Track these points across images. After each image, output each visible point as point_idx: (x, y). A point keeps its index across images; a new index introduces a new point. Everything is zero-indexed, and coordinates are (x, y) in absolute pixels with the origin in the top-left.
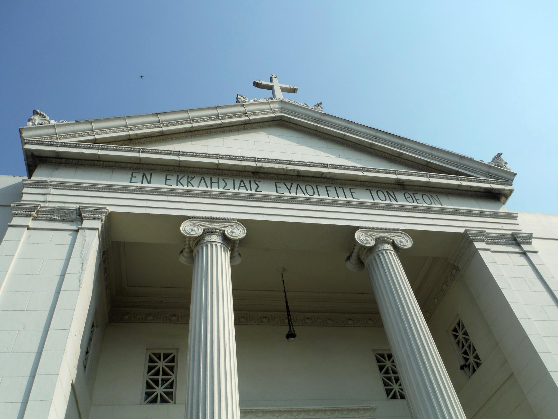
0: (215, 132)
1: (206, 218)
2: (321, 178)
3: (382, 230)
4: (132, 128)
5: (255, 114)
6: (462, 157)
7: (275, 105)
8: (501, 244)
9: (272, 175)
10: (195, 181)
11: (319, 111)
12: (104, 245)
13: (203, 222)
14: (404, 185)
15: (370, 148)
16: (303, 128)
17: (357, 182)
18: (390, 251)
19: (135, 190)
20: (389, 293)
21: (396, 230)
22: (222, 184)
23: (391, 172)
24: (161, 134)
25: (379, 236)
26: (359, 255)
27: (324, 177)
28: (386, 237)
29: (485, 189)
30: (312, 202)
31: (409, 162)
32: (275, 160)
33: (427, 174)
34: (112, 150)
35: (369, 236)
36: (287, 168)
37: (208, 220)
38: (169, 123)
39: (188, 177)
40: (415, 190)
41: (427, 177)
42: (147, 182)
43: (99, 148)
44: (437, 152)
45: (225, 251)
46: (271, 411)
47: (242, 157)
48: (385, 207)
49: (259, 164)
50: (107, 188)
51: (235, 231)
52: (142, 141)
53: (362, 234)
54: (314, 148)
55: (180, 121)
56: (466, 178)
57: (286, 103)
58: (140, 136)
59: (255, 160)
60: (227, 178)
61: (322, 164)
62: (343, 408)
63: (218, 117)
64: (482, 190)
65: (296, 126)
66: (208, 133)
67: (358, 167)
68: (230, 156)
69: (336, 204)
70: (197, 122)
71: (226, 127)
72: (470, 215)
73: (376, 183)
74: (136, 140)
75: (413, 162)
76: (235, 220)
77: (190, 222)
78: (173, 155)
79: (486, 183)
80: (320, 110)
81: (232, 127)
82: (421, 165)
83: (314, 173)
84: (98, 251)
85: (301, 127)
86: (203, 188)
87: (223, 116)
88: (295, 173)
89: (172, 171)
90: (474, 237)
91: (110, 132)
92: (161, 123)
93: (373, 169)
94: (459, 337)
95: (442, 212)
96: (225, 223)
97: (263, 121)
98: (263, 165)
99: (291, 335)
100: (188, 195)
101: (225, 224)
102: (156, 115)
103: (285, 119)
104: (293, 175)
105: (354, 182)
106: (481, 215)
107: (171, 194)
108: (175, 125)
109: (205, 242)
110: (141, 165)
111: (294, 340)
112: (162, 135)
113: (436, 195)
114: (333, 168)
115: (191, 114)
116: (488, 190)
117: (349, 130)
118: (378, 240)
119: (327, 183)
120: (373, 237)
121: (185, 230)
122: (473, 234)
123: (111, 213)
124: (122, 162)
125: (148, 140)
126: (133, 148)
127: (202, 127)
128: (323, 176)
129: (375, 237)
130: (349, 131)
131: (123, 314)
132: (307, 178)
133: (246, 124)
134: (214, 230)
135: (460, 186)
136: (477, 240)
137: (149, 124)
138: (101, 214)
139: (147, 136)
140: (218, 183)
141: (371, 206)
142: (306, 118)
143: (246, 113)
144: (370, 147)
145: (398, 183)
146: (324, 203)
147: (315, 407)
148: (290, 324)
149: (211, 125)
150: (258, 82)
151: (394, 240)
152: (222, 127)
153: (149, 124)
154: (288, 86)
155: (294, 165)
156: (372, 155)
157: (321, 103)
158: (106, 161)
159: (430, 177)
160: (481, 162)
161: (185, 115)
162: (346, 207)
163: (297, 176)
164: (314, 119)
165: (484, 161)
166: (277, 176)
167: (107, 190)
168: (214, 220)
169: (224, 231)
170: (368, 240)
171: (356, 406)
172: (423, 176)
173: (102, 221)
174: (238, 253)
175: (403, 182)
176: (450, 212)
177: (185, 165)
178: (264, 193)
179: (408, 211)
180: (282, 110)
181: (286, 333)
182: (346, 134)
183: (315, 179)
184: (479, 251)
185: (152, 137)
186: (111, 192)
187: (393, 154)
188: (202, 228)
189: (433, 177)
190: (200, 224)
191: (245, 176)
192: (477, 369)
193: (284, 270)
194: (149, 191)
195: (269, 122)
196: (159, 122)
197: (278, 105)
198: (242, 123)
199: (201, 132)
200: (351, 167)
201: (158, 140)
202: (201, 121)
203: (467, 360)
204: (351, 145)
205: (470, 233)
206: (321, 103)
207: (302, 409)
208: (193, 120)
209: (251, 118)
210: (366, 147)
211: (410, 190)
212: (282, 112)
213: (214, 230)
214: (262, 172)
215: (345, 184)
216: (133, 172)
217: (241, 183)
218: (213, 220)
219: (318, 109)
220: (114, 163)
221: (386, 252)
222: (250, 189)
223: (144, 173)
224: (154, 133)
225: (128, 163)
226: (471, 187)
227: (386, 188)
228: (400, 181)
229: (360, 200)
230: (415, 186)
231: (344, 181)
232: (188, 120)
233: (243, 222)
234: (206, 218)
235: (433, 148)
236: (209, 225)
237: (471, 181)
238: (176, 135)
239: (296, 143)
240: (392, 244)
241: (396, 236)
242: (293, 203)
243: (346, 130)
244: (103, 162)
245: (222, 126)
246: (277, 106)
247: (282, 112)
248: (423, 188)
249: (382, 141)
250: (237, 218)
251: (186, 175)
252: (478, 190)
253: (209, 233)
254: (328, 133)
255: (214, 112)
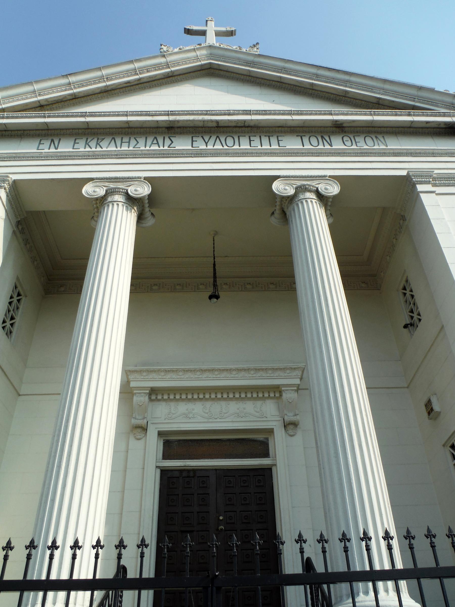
0: (134, 90)
1: (110, 178)
2: (245, 127)
3: (306, 177)
4: (41, 93)
5: (178, 64)
6: (420, 88)
7: (201, 51)
8: (452, 186)
9: (188, 129)
10: (104, 143)
11: (254, 53)
12: (16, 214)
13: (107, 183)
14: (343, 127)
15: (311, 89)
16: (235, 75)
17: (286, 129)
18: (312, 200)
19: (39, 156)
20: (301, 243)
21: (322, 177)
22: (133, 142)
23: (326, 113)
24: (74, 97)
25: (299, 184)
26: (283, 208)
27: (247, 125)
28: (307, 185)
29: (445, 123)
30: (229, 154)
31: (357, 101)
32: (191, 111)
33: (371, 111)
34: (18, 118)
35: (289, 185)
36: (203, 119)
37: (113, 180)
38: (80, 84)
39: (98, 139)
40: (357, 132)
41: (371, 115)
42: (54, 148)
43: (4, 117)
44: (390, 85)
45: (127, 210)
46: (192, 371)
47: (154, 111)
48: (314, 152)
49: (172, 118)
50: (12, 157)
51: (138, 189)
52: (54, 106)
53: (281, 183)
54: (245, 96)
55: (93, 81)
56: (421, 112)
57: (215, 47)
58: (51, 101)
59: (169, 114)
60: (139, 136)
61: (244, 111)
62: (268, 367)
63: (135, 72)
64: (442, 126)
65: (227, 73)
66: (126, 91)
67: (287, 111)
68: (140, 112)
69: (257, 153)
70: (112, 79)
71: (146, 82)
72: (420, 155)
73: (308, 127)
74: (48, 106)
75: (362, 100)
76: (140, 178)
77: (93, 184)
78: (80, 117)
79: (447, 117)
80: (254, 52)
81: (153, 82)
82: (371, 103)
83: (235, 122)
84: (5, 219)
85: (232, 74)
86: (112, 148)
87: (142, 70)
88: (215, 125)
89: (81, 134)
90: (417, 178)
91: (18, 100)
92: (72, 85)
93: (305, 111)
94: (407, 294)
95: (385, 153)
96: (130, 182)
97: (190, 71)
98: (176, 118)
99: (214, 296)
100: (94, 156)
101: (130, 183)
102: (66, 76)
103: (215, 67)
104: (212, 126)
105: (283, 129)
106: (433, 154)
107: (77, 158)
108: (87, 86)
109: (107, 203)
110: (49, 131)
111: (217, 302)
112: (75, 98)
113: (382, 135)
114: (256, 114)
115: (105, 72)
116: (449, 125)
117: (286, 71)
118: (299, 188)
119: (251, 132)
120: (293, 185)
121: (87, 192)
122: (416, 176)
123: (15, 181)
124: (30, 130)
125: (60, 105)
126: (39, 114)
127: (119, 85)
128: (246, 124)
129: (296, 186)
130: (286, 72)
131: (59, 286)
132: (228, 128)
133: (169, 77)
134: (117, 190)
135: (412, 122)
136: (421, 183)
137: (59, 88)
138: (4, 182)
139: (60, 101)
140: (129, 142)
141: (298, 153)
142: (237, 62)
143: (168, 65)
144: (312, 88)
145: (336, 126)
146: (243, 153)
147: (237, 366)
148: (215, 285)
149: (128, 82)
150: (189, 28)
151: (318, 187)
152: (141, 84)
153: (59, 88)
154: (223, 29)
155: (212, 115)
156: (313, 97)
157: (257, 44)
158: (14, 131)
159: (375, 115)
160: (445, 92)
161: (98, 74)
162: (268, 156)
163: (216, 127)
164: (247, 63)
165: (449, 90)
166: (194, 129)
167: (12, 159)
168: (118, 180)
169: (127, 190)
170: (287, 190)
171: (281, 365)
172: (365, 115)
173: (5, 189)
174: (151, 213)
175: (342, 124)
176: (394, 153)
177: (94, 127)
178: (177, 148)
179: (342, 155)
180: (211, 56)
181: (210, 293)
182: (281, 75)
183: (237, 129)
184: (421, 194)
185: (64, 101)
186: (16, 160)
187: (338, 94)
188: (105, 188)
189: (378, 115)
190: (101, 184)
191: (159, 133)
192: (419, 324)
193: (216, 233)
194: (54, 156)
195: (196, 73)
196: (69, 84)
197: (206, 51)
198: (165, 77)
199: (118, 90)
200: (278, 111)
201: (71, 104)
202: (116, 79)
203: (412, 317)
204: (268, 84)
205: (413, 175)
206: (257, 44)
207: (223, 368)
208: (108, 78)
209: (173, 69)
210: (307, 88)
211: (351, 132)
212: (211, 59)
213: (117, 190)
214: (177, 126)
215: (272, 132)
216: (41, 138)
217: (154, 141)
218: (118, 180)
219: (253, 50)
220: (22, 132)
221: (306, 201)
222: (162, 146)
223: (53, 139)
224: (65, 96)
225: (36, 130)
226: (427, 122)
227: (321, 132)
228: (338, 123)
229: (287, 147)
230: (357, 127)
231: (271, 129)
232: (101, 79)
233: (149, 179)
234: (110, 178)
235: (385, 81)
236: (112, 185)
237: (427, 116)
238: (90, 97)
239: (225, 92)
240: (316, 192)
241: (320, 183)
242: (207, 157)
243: (283, 71)
244: (11, 132)
245: (141, 82)
246: (204, 52)
247: (210, 58)
248: (367, 129)
249: (325, 79)
250: (142, 176)
251: (96, 137)
252: (437, 126)
253: (112, 193)
254: (262, 77)
255: (131, 66)
